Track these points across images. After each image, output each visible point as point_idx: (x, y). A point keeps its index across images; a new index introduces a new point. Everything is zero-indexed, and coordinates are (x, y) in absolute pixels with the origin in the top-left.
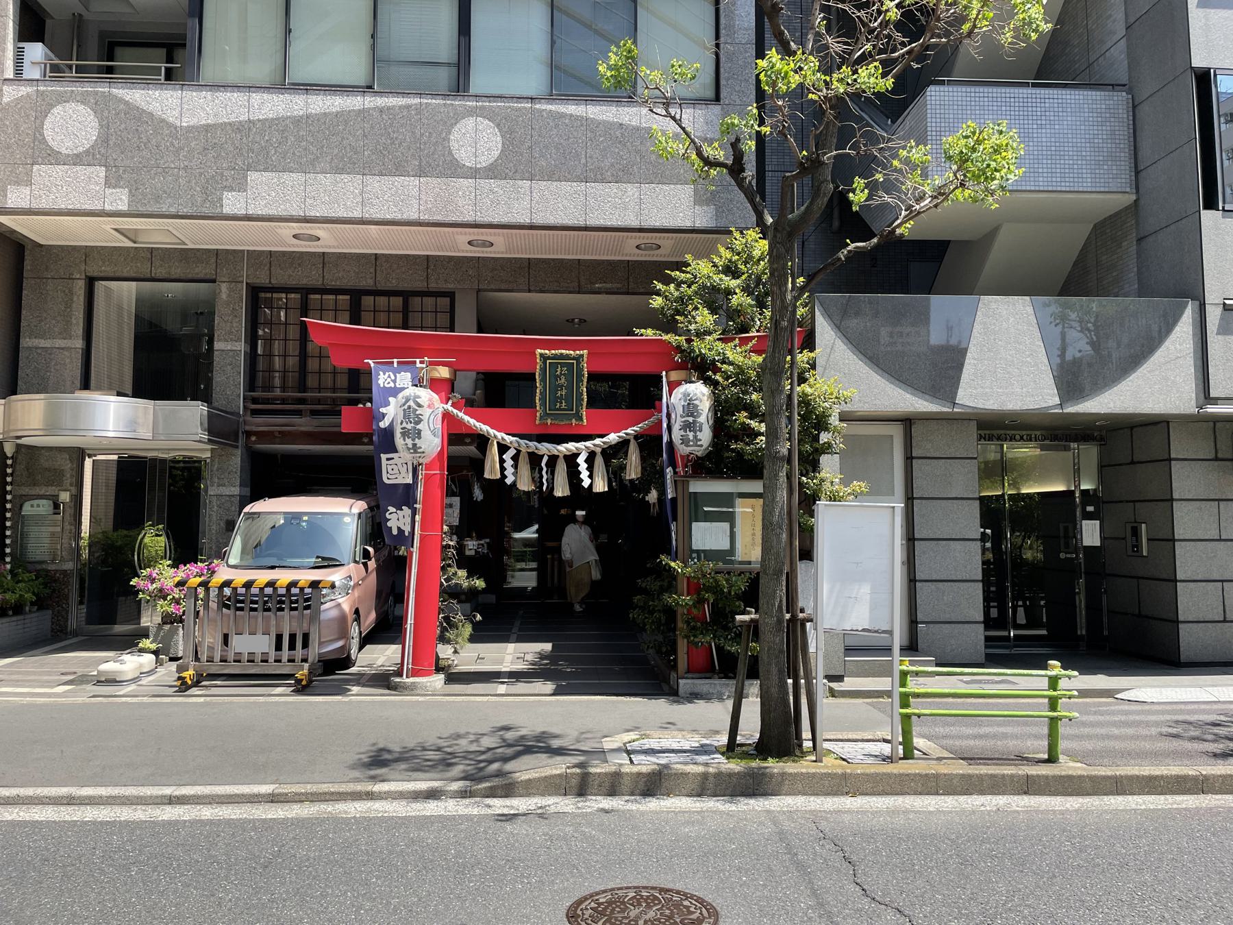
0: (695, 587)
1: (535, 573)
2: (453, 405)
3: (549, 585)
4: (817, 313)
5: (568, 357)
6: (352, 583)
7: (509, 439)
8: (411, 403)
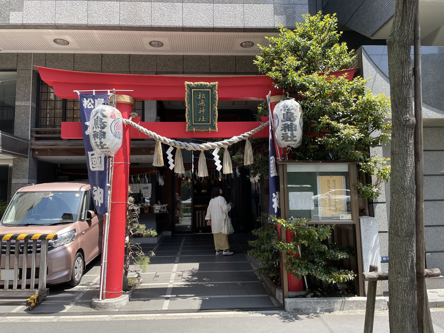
0: (292, 236)
1: (190, 218)
2: (133, 120)
3: (197, 226)
4: (364, 57)
5: (205, 87)
6: (76, 234)
7: (168, 140)
8: (99, 115)
